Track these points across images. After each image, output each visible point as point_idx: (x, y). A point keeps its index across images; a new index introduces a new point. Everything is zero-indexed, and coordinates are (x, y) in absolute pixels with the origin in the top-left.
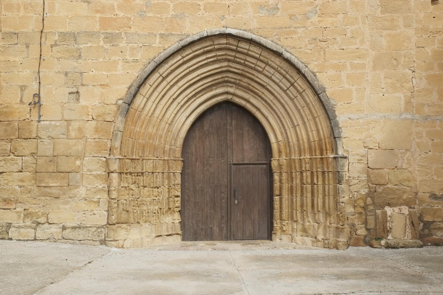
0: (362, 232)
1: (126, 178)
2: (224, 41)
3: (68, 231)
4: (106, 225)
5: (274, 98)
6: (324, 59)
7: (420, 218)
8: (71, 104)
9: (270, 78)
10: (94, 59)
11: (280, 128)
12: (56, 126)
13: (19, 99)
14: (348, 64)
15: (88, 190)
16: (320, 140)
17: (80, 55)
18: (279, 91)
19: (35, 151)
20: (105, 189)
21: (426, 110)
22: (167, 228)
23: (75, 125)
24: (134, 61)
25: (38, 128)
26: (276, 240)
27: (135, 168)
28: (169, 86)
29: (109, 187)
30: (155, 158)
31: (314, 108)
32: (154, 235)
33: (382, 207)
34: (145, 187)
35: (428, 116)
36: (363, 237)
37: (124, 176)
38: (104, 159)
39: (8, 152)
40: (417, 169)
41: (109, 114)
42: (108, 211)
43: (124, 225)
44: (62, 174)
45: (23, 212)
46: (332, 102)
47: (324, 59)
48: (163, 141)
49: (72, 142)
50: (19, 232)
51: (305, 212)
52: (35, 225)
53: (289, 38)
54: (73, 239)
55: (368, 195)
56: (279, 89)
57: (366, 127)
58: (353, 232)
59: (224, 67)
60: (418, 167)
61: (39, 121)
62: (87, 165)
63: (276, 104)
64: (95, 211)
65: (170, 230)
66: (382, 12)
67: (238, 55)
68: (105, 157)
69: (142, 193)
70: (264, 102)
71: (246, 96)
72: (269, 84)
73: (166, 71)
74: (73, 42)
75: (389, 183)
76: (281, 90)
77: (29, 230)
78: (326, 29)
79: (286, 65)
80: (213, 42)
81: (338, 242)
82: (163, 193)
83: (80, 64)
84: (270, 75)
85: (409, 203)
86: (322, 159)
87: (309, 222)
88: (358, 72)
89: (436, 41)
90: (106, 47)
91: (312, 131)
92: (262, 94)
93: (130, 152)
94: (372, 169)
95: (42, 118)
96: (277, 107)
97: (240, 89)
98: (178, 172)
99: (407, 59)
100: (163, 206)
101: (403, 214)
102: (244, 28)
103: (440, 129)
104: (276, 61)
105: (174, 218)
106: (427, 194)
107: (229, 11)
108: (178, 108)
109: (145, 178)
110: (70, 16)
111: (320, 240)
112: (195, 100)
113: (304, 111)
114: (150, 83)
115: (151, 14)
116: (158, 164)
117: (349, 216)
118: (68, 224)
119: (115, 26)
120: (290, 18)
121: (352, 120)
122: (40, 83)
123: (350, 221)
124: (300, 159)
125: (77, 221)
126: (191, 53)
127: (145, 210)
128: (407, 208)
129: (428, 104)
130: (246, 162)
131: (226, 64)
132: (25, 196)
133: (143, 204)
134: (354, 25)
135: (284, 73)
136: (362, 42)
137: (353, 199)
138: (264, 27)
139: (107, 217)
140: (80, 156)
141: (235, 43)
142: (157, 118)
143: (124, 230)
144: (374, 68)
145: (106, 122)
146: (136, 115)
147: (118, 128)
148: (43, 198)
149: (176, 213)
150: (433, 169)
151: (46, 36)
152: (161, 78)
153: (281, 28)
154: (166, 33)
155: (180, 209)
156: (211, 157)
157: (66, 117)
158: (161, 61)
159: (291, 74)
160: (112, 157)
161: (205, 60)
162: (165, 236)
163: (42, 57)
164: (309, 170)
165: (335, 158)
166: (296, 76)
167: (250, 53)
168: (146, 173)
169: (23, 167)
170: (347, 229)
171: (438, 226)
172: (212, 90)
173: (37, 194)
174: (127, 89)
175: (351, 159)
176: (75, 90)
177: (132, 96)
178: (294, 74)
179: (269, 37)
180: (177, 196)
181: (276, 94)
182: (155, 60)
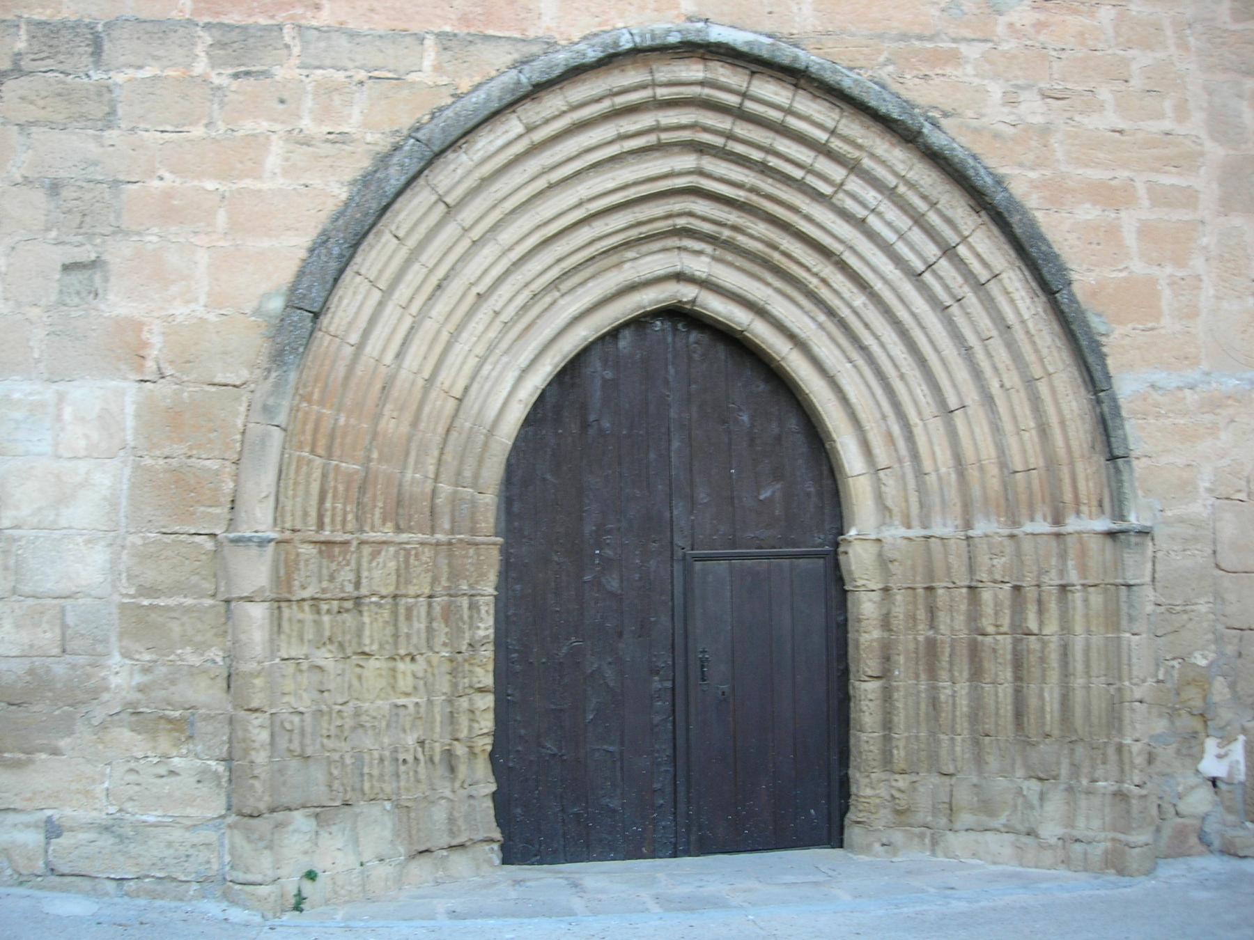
1: (299, 621)
2: (693, 70)
5: (867, 302)
8: (74, 314)
9: (860, 224)
10: (169, 128)
11: (884, 417)
14: (1141, 190)
16: (1051, 464)
17: (113, 112)
24: (330, 137)
27: (332, 578)
31: (1034, 343)
38: (209, 545)
53: (934, 76)
54: (94, 875)
63: (872, 326)
64: (176, 760)
67: (743, 130)
70: (822, 318)
72: (852, 248)
74: (87, 60)
78: (1064, 55)
79: (929, 176)
80: (651, 72)
81: (1127, 848)
83: (112, 148)
84: (860, 212)
91: (1019, 431)
92: (821, 285)
96: (877, 338)
97: (730, 264)
100: (432, 729)
108: (492, 334)
113: (989, 356)
114: (398, 228)
116: (417, 563)
121: (1160, 392)
124: (968, 538)
125: (104, 801)
131: (688, 161)
135: (922, 206)
137: (1169, 685)
145: (213, 389)
153: (904, 37)
154: (462, 31)
159: (949, 213)
162: (445, 853)
164: (1006, 579)
168: (374, 599)
174: (303, 254)
178: (960, 211)
179: (861, 68)
181: (878, 286)
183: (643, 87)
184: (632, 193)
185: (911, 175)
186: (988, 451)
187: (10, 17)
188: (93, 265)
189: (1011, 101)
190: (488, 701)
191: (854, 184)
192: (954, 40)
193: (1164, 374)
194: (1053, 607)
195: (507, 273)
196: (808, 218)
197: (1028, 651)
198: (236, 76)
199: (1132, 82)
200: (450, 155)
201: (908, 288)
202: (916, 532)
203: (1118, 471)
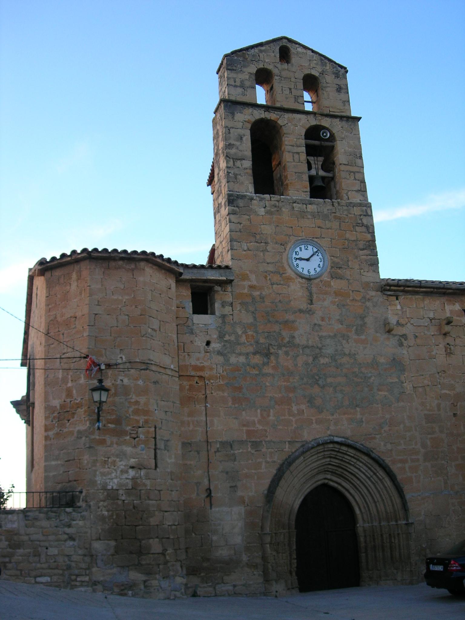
17: (235, 458)
46: (402, 485)
70: (351, 485)
86: (397, 525)
110: (225, 429)
131: (328, 459)
153: (366, 435)
159: (375, 468)
174: (270, 483)
181: (362, 480)
185: (368, 461)
186: (383, 509)
187: (215, 441)
188: (236, 486)
189: (385, 445)
190: (295, 561)
191: (358, 463)
192: (375, 435)
194: (397, 537)
196: (350, 468)
198: (256, 451)
201: (367, 480)
202: (370, 525)
203: (407, 513)
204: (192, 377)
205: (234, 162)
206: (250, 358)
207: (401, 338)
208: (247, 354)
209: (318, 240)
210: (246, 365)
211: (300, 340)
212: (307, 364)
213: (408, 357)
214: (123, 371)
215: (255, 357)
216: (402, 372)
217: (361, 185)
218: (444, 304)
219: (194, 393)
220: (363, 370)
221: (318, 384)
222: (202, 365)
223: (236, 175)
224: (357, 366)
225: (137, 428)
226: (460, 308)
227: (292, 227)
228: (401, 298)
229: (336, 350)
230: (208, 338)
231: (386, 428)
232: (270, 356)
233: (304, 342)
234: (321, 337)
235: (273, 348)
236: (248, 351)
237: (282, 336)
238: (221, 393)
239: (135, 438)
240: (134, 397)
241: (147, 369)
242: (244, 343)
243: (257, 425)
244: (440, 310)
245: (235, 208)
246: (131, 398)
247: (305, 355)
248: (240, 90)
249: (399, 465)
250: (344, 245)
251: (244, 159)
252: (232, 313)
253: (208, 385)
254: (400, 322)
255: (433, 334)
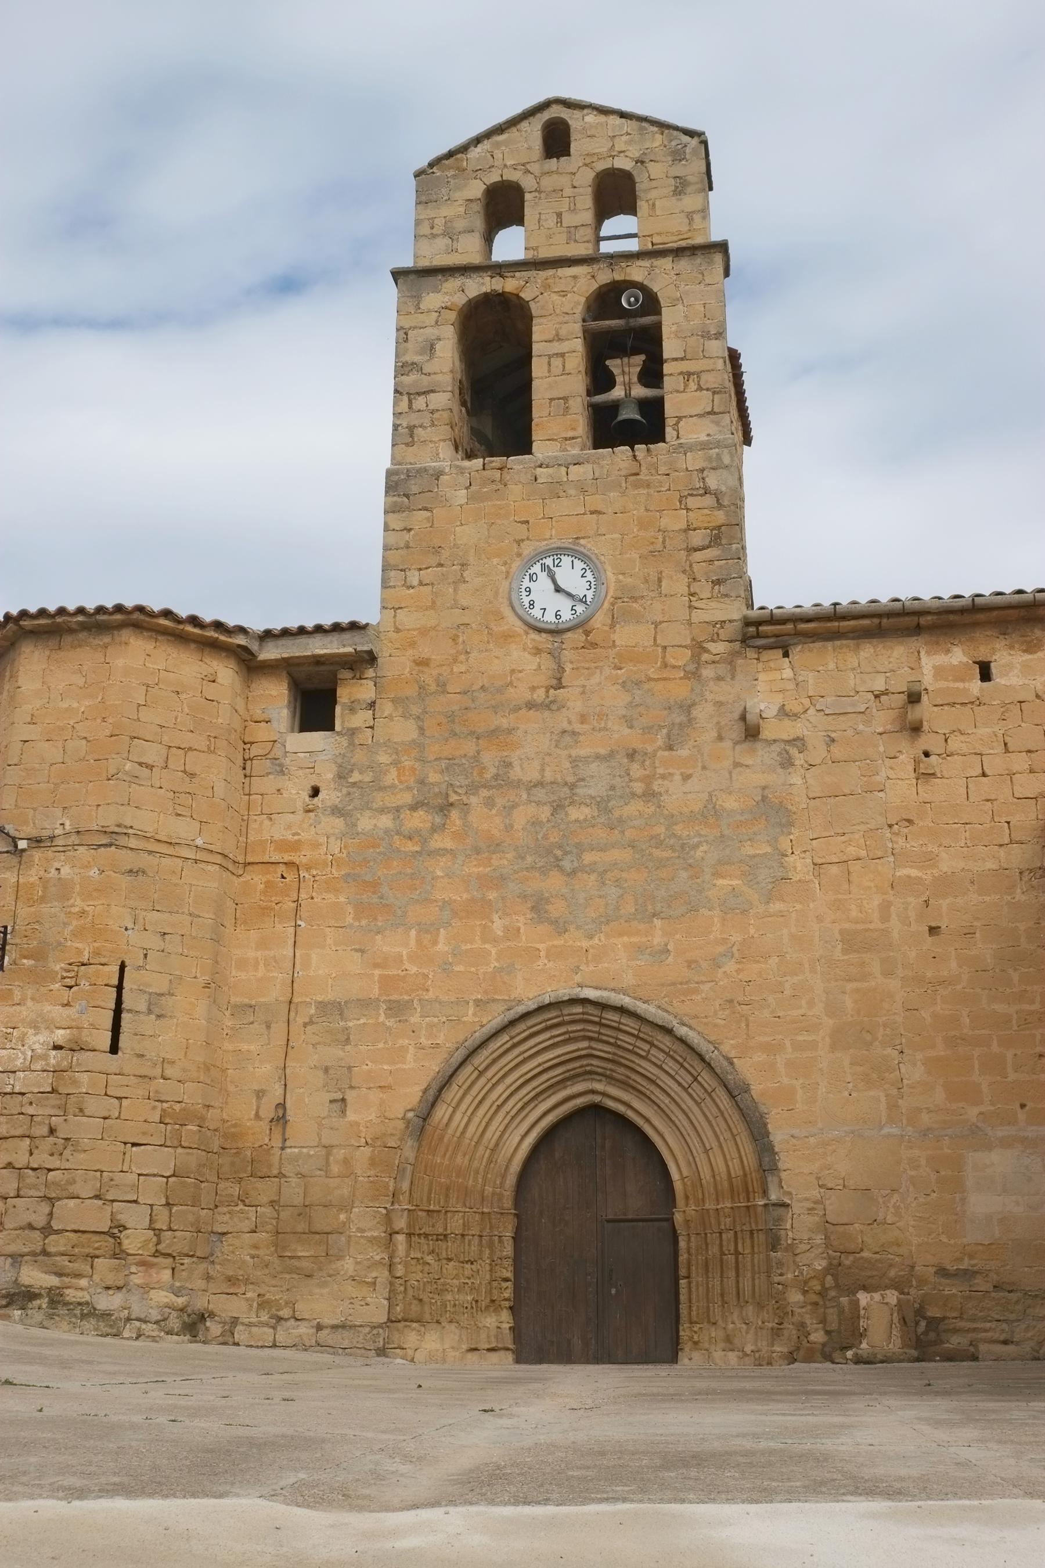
0: (818, 1337)
2: (578, 1009)
3: (325, 1332)
4: (385, 1323)
6: (748, 1035)
7: (920, 1312)
9: (660, 1067)
12: (311, 1156)
13: (254, 1112)
14: (788, 1043)
15: (357, 1263)
16: (745, 1175)
17: (348, 1039)
18: (676, 1090)
19: (276, 1198)
20: (384, 1261)
21: (925, 1118)
22: (488, 1337)
23: (339, 1154)
25: (281, 1159)
26: (683, 1359)
27: (433, 1226)
28: (490, 1085)
29: (391, 1258)
30: (468, 1210)
32: (465, 1347)
33: (852, 1292)
34: (450, 1260)
35: (928, 1129)
36: (820, 1347)
37: (415, 1239)
38: (384, 1211)
39: (236, 1199)
40: (912, 1223)
41: (392, 1135)
42: (389, 1299)
43: (414, 1325)
44: (318, 1236)
45: (256, 1298)
46: (763, 1109)
47: (748, 1035)
48: (480, 1180)
49: (333, 1183)
50: (250, 1333)
51: (726, 1305)
52: (274, 1321)
55: (827, 1271)
56: (676, 1085)
57: (821, 1151)
58: (802, 1338)
59: (582, 1049)
60: (914, 1220)
61: (283, 1149)
62: (356, 1221)
65: (493, 1339)
66: (845, 951)
68: (385, 1208)
69: (444, 1271)
71: (625, 1096)
73: (484, 1061)
74: (338, 1017)
75: (865, 1250)
76: (680, 1088)
77: (266, 1329)
78: (750, 984)
82: (481, 1272)
84: (659, 1063)
85: (898, 1285)
87: (733, 1323)
88: (805, 1056)
89: (939, 997)
90: (388, 1024)
93: (425, 1199)
94: (833, 1225)
95: (288, 1144)
98: (507, 1234)
99: (888, 1031)
101: (887, 1304)
102: (612, 985)
103: (950, 1151)
104: (666, 1041)
105: (501, 1320)
106: (930, 1268)
107: (587, 958)
108: (506, 1121)
109: (449, 1244)
110: (334, 975)
111: (749, 1352)
112: (536, 1106)
115: (460, 968)
117: (794, 1309)
118: (327, 1321)
119: (403, 988)
120: (689, 967)
122: (285, 1085)
123: (796, 1319)
126: (525, 1031)
127: (449, 1301)
128: (896, 1293)
129: (927, 1108)
130: (630, 1217)
131: (585, 1044)
132: (259, 1273)
133: (447, 1290)
134: (797, 976)
136: (811, 1004)
137: (801, 1278)
138: (646, 984)
139: (387, 1309)
140: (346, 1206)
141: (597, 1012)
142: (453, 1136)
143: (414, 1332)
144: (833, 1047)
146: (436, 1137)
147: (407, 1159)
148: (288, 1276)
149: (505, 1310)
150: (940, 1223)
151: (296, 1009)
152: (476, 1073)
153: (673, 984)
154: (485, 998)
155: (512, 1304)
156: (568, 1208)
157: (324, 1142)
158: (476, 1046)
159: (691, 1063)
160: (396, 1206)
161: (549, 1039)
163: (291, 1044)
165: (766, 1205)
166: (699, 1066)
167: (621, 1027)
169: (258, 1225)
170: (790, 1330)
171: (952, 1326)
172: (565, 1088)
173: (279, 1269)
174: (421, 1094)
175: (797, 1208)
176: (339, 1096)
177: (430, 1105)
178: (696, 1062)
180: (506, 1280)
181: (673, 1094)
182: (466, 1044)
183: (559, 1016)
184: (562, 1059)
193: (798, 1131)
195: (512, 1094)
196: (639, 1065)
197: (240, 1120)
199: (785, 992)
200: (479, 1051)
204: (273, 866)
205: (410, 401)
206: (402, 817)
207: (788, 748)
208: (398, 809)
209: (589, 542)
210: (392, 833)
211: (525, 771)
212: (536, 823)
213: (805, 791)
214: (64, 851)
215: (415, 814)
216: (784, 830)
217: (713, 401)
218: (919, 652)
219: (273, 899)
220: (678, 829)
221: (561, 869)
222: (296, 838)
223: (411, 429)
224: (662, 821)
225: (78, 966)
226: (965, 659)
227: (528, 522)
228: (796, 651)
229: (613, 788)
230: (314, 781)
231: (730, 967)
232: (449, 811)
233: (532, 774)
234: (575, 761)
235: (456, 792)
236: (400, 803)
237: (482, 763)
238: (331, 897)
239: (71, 987)
240: (78, 902)
241: (111, 845)
242: (393, 786)
243: (407, 965)
244: (906, 669)
245: (399, 500)
246: (73, 906)
247: (533, 804)
248: (442, 242)
249: (760, 1057)
250: (652, 543)
251: (433, 391)
252: (372, 724)
253: (304, 881)
254: (787, 708)
255: (880, 730)
